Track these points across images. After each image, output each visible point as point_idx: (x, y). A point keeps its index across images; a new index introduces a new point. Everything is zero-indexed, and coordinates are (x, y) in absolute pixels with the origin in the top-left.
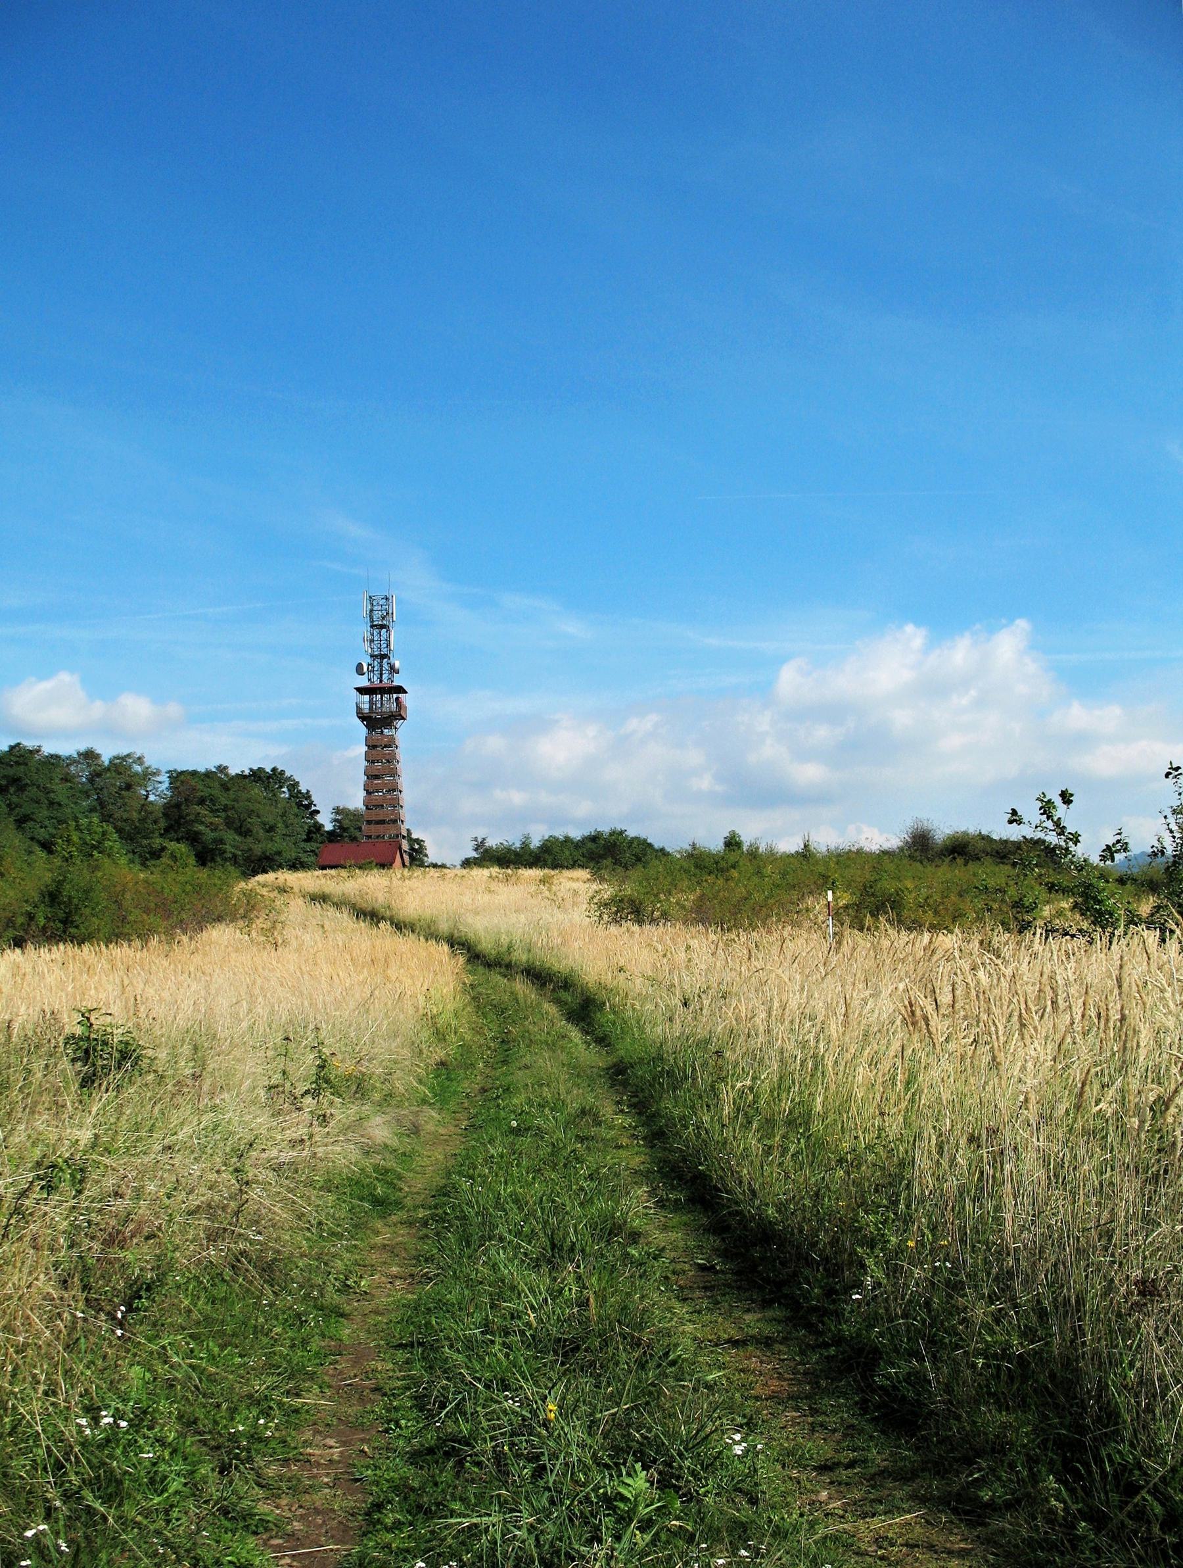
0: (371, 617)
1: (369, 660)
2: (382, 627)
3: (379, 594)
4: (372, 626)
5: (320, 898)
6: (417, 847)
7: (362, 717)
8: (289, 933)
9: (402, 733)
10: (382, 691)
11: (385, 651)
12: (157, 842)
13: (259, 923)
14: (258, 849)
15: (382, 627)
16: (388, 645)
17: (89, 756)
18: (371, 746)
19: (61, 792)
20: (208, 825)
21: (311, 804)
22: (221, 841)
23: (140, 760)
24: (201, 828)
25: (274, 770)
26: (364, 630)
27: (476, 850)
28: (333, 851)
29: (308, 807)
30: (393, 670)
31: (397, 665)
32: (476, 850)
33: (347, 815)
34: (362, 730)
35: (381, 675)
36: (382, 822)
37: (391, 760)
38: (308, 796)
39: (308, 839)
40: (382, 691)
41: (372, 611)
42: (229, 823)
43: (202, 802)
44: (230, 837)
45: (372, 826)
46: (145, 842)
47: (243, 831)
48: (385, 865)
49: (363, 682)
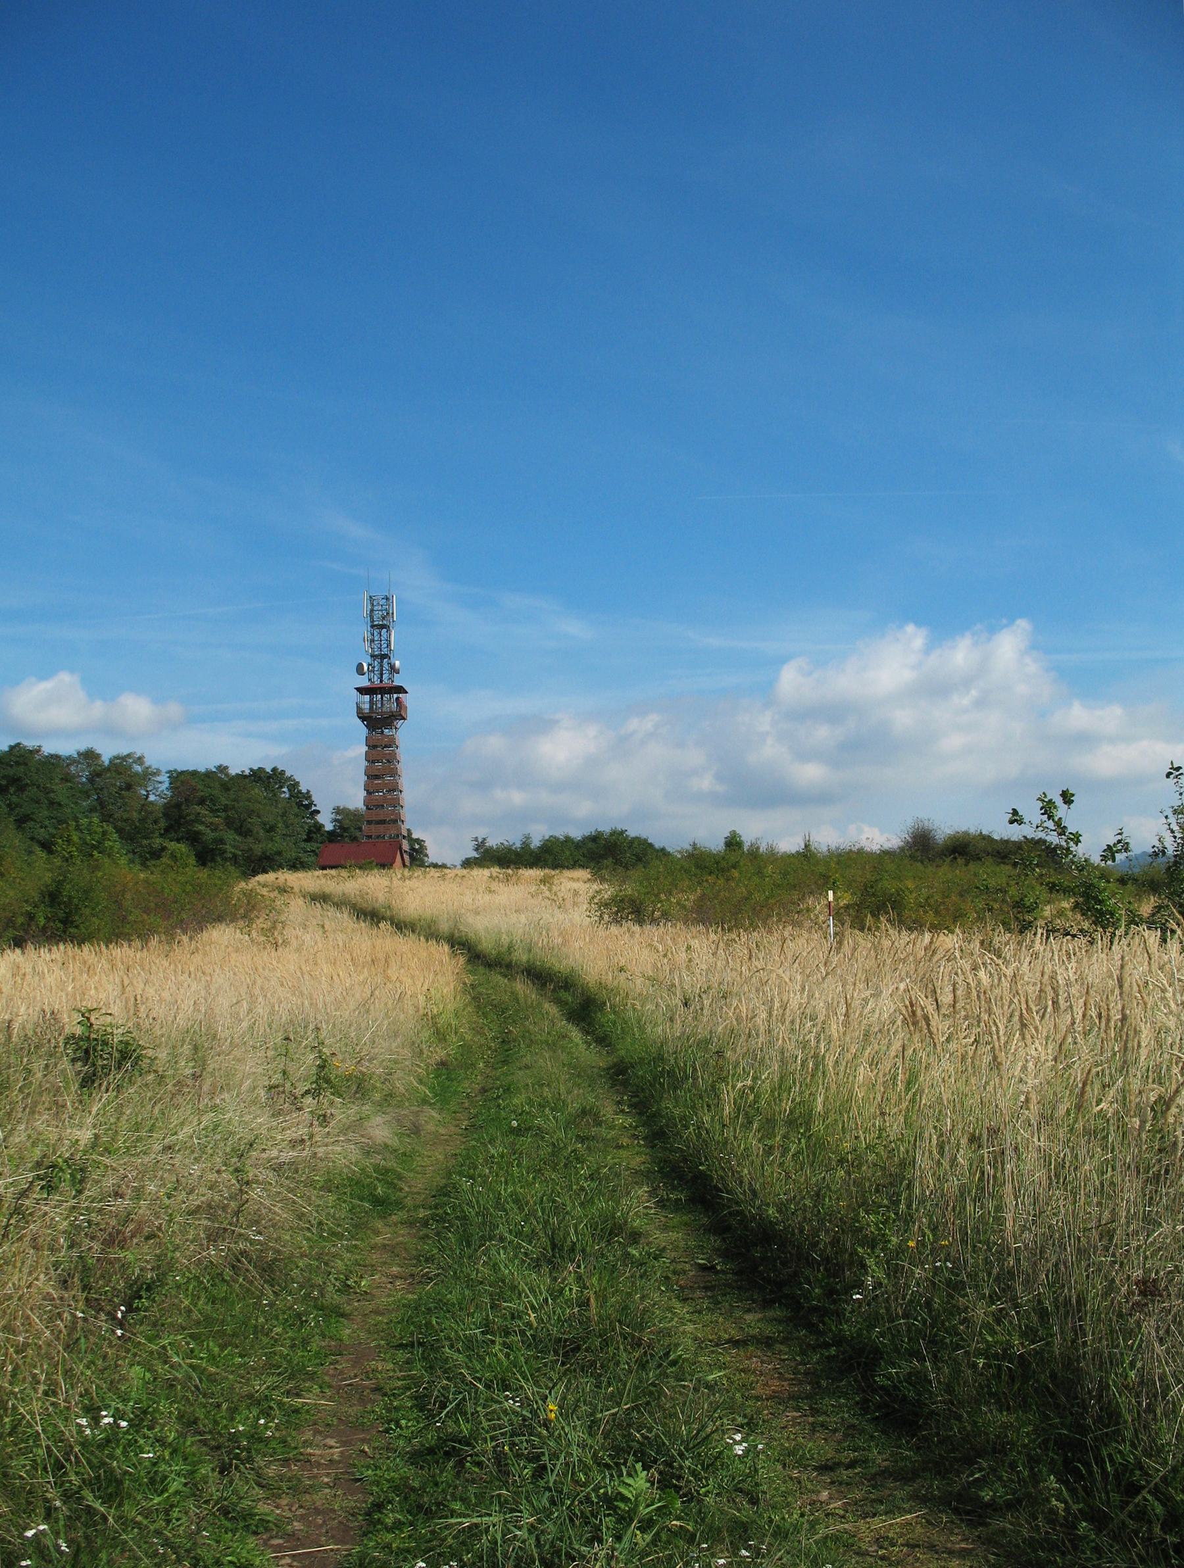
0: (372, 617)
1: (369, 660)
2: (383, 627)
3: (379, 593)
4: (372, 626)
5: (320, 898)
6: (417, 847)
7: (363, 717)
9: (404, 735)
10: (382, 690)
11: (385, 651)
13: (260, 923)
14: (258, 849)
16: (389, 645)
17: (89, 756)
18: (372, 746)
19: (60, 791)
20: (209, 825)
21: (311, 804)
22: (221, 841)
24: (201, 828)
25: (274, 769)
26: (364, 630)
27: (476, 850)
29: (308, 807)
30: (393, 670)
31: (397, 664)
34: (362, 730)
35: (382, 674)
38: (308, 796)
39: (309, 839)
40: (382, 690)
41: (372, 611)
42: (229, 823)
43: (202, 802)
44: (230, 836)
45: (373, 826)
46: (145, 842)
49: (364, 682)
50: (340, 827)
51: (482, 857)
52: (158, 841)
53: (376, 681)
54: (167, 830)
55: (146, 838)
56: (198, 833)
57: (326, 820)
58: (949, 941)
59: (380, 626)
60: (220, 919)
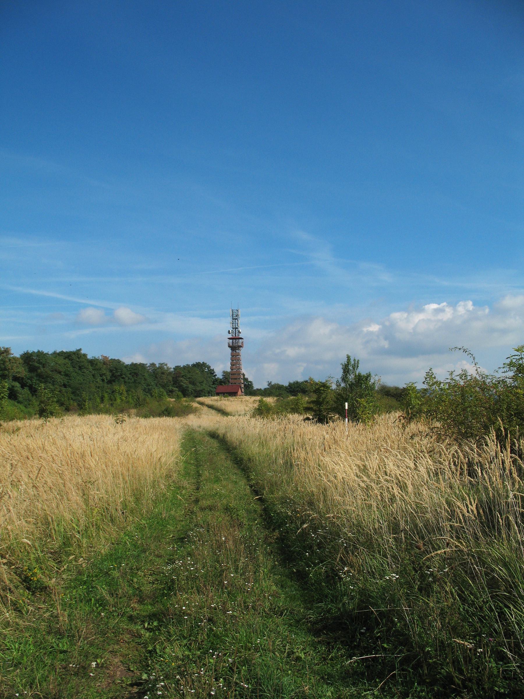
0: (233, 316)
1: (232, 329)
2: (236, 319)
3: (235, 308)
4: (233, 319)
5: (210, 407)
6: (250, 384)
7: (229, 346)
8: (203, 416)
9: (242, 352)
10: (236, 339)
11: (237, 327)
12: (171, 388)
13: (197, 414)
14: (198, 389)
15: (236, 319)
16: (238, 325)
17: (153, 365)
18: (232, 356)
19: (146, 375)
20: (185, 383)
21: (214, 372)
22: (188, 387)
23: (166, 365)
24: (182, 384)
25: (203, 363)
26: (230, 319)
27: (268, 385)
28: (221, 389)
29: (213, 373)
30: (239, 332)
31: (240, 330)
32: (268, 385)
33: (227, 374)
34: (229, 350)
35: (236, 334)
36: (236, 379)
37: (239, 360)
38: (213, 370)
39: (214, 384)
40: (236, 339)
41: (233, 314)
42: (190, 383)
43: (183, 377)
44: (190, 386)
45: (233, 380)
46: (168, 388)
47: (193, 383)
48: (234, 394)
49: (230, 336)
50: (225, 378)
51: (270, 388)
52: (171, 387)
53: (234, 336)
54: (173, 384)
55: (168, 387)
56: (182, 385)
57: (219, 375)
58: (26, 421)
59: (235, 318)
60: (190, 413)
